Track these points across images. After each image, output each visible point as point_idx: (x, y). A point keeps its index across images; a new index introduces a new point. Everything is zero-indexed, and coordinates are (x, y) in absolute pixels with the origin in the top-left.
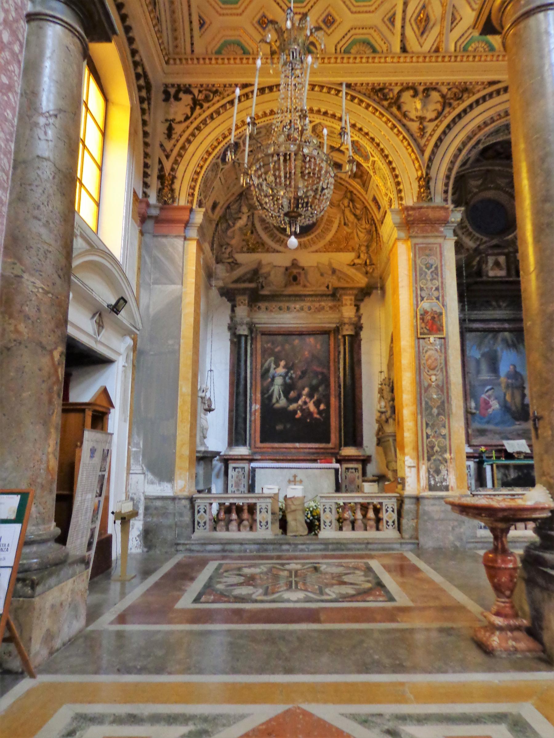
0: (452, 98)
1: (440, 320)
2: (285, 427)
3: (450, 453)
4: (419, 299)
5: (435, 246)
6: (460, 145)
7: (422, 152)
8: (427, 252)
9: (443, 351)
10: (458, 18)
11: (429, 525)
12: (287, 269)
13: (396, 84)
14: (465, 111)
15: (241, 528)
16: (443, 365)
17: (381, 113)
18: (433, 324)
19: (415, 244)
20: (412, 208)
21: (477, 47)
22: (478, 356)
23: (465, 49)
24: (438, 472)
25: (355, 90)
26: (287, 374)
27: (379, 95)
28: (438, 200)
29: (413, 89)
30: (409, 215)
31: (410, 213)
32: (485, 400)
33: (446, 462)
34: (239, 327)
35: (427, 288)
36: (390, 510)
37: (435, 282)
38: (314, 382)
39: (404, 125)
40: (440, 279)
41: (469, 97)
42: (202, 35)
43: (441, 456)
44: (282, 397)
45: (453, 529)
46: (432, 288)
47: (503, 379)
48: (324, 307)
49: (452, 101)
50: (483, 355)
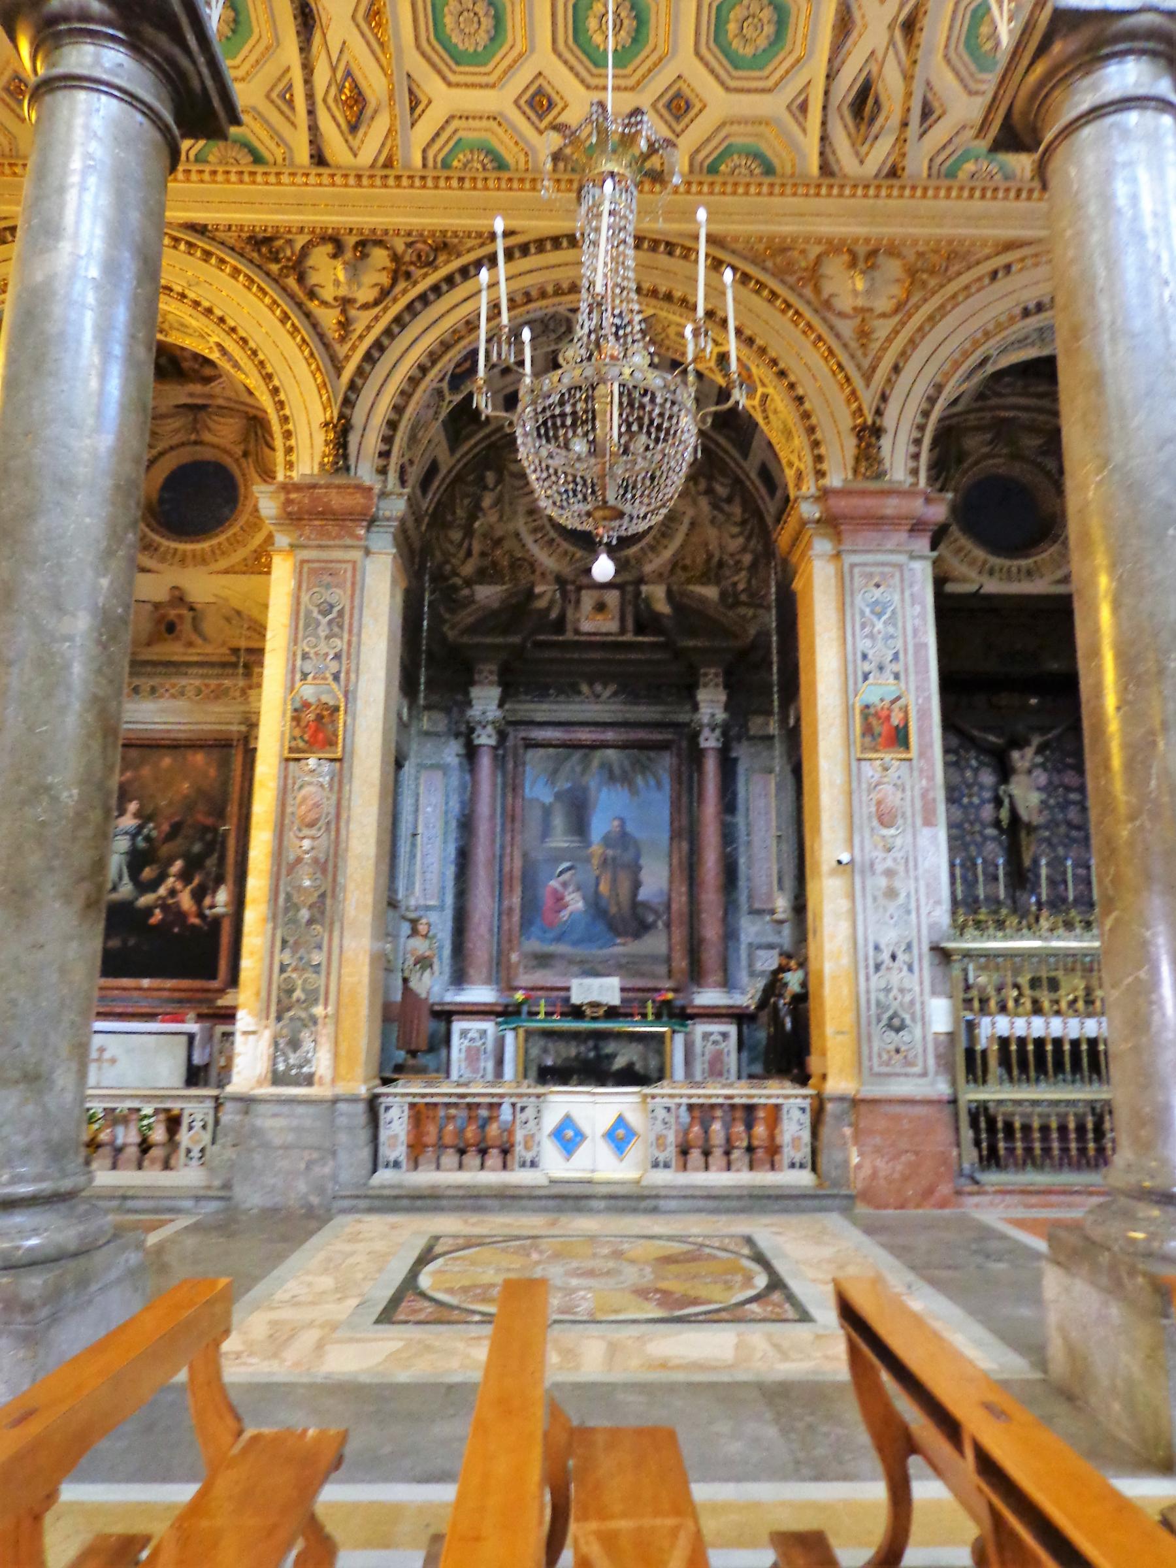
0: (412, 263)
1: (333, 722)
2: (124, 942)
3: (326, 1005)
4: (298, 676)
5: (344, 566)
6: (424, 360)
7: (339, 370)
8: (327, 579)
9: (336, 787)
10: (424, 102)
11: (258, 1158)
12: (157, 606)
13: (301, 230)
14: (436, 289)
15: (146, 1163)
16: (332, 816)
17: (260, 289)
18: (317, 730)
19: (303, 562)
20: (837, 493)
21: (468, 162)
22: (548, 799)
23: (446, 165)
24: (295, 1044)
25: (213, 239)
26: (140, 828)
27: (264, 250)
28: (365, 472)
29: (335, 242)
30: (288, 502)
31: (293, 496)
32: (555, 891)
33: (315, 1023)
34: (479, 730)
35: (316, 654)
36: (198, 1125)
37: (337, 642)
38: (197, 848)
39: (308, 315)
40: (346, 636)
41: (447, 262)
42: (925, 132)
43: (306, 1009)
44: (126, 879)
45: (308, 1168)
46: (327, 654)
47: (596, 848)
48: (228, 689)
49: (412, 268)
50: (558, 796)
